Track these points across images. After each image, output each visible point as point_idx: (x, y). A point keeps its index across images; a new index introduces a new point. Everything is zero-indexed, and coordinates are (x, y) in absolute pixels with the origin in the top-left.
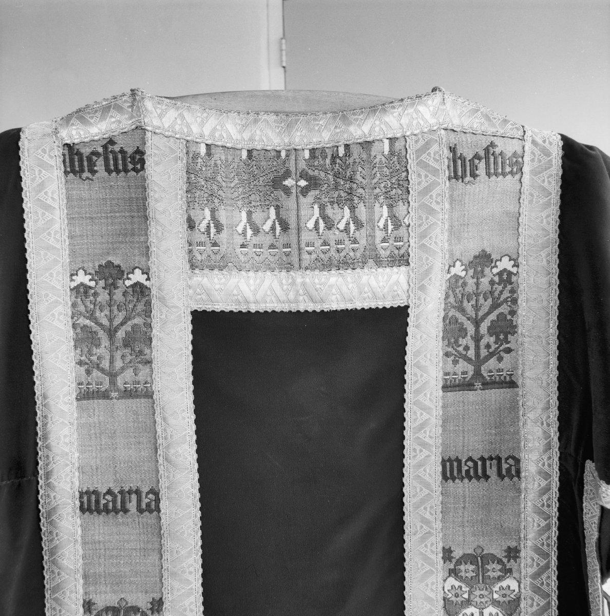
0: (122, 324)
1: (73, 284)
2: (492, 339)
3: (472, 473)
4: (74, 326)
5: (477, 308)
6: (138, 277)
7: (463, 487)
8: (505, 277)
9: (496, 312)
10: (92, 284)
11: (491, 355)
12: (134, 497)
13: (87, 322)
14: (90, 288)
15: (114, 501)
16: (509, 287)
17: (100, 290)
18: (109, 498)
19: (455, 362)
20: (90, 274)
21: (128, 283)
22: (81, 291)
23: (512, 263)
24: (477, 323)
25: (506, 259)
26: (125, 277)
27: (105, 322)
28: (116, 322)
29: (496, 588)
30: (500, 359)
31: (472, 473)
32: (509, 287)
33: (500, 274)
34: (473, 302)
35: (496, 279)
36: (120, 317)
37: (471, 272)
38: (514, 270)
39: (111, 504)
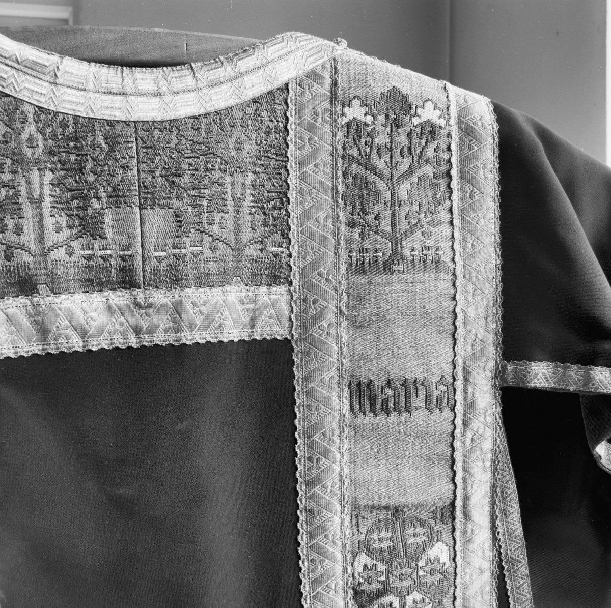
0: (403, 176)
5: (392, 166)
10: (369, 119)
13: (362, 171)
14: (366, 124)
15: (396, 396)
18: (390, 392)
21: (416, 121)
23: (438, 113)
27: (387, 172)
28: (397, 173)
29: (422, 563)
32: (433, 145)
36: (405, 164)
37: (381, 118)
38: (442, 122)
39: (392, 400)
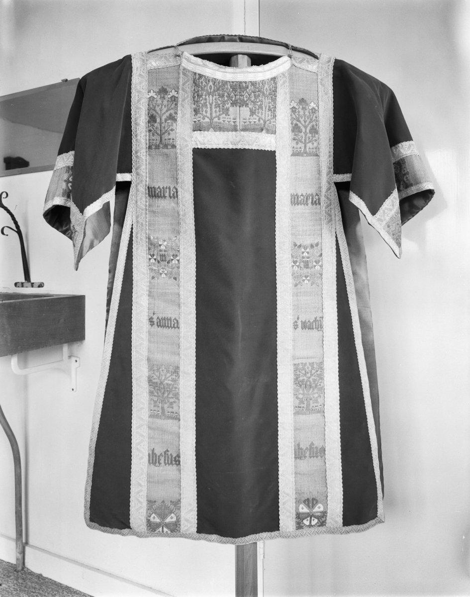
1: (149, 96)
2: (310, 135)
3: (317, 202)
4: (292, 124)
6: (173, 93)
7: (300, 208)
8: (173, 99)
9: (169, 112)
11: (310, 142)
12: (168, 190)
15: (160, 192)
16: (175, 103)
17: (300, 110)
19: (297, 143)
20: (155, 92)
21: (169, 96)
22: (293, 110)
24: (306, 127)
25: (173, 91)
26: (299, 104)
30: (313, 144)
31: (317, 202)
33: (171, 97)
34: (160, 107)
35: (170, 100)
38: (177, 96)
